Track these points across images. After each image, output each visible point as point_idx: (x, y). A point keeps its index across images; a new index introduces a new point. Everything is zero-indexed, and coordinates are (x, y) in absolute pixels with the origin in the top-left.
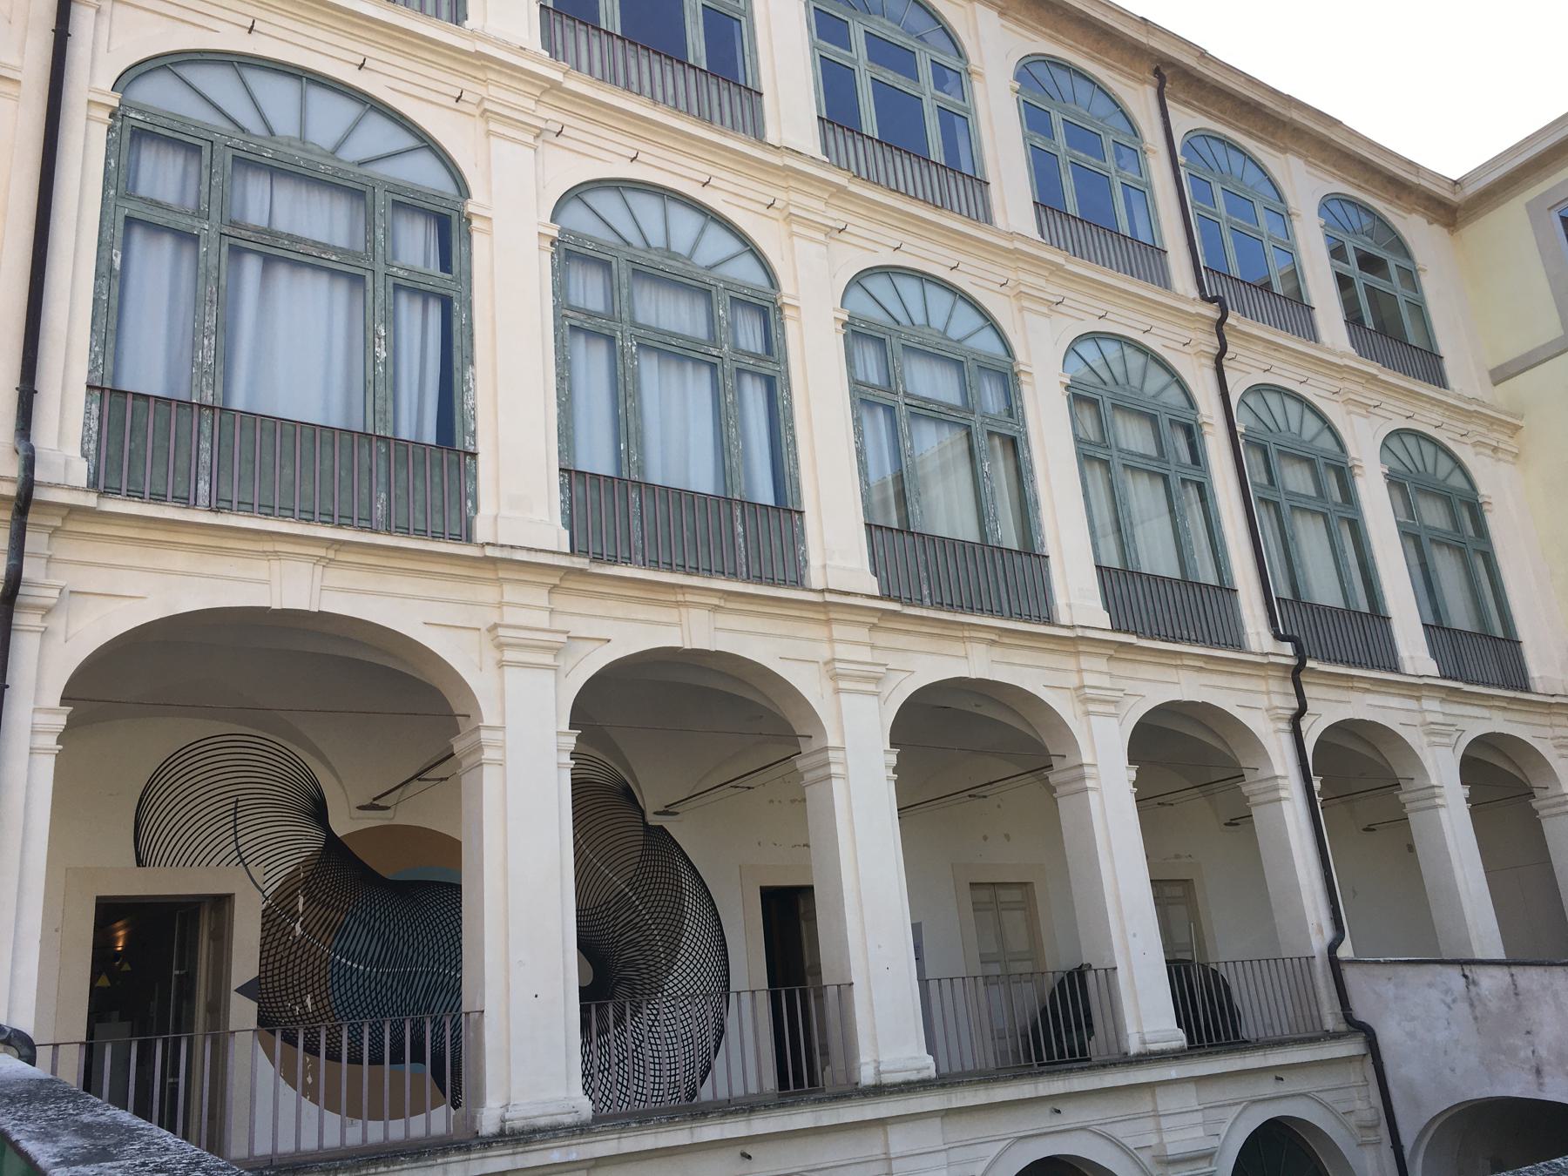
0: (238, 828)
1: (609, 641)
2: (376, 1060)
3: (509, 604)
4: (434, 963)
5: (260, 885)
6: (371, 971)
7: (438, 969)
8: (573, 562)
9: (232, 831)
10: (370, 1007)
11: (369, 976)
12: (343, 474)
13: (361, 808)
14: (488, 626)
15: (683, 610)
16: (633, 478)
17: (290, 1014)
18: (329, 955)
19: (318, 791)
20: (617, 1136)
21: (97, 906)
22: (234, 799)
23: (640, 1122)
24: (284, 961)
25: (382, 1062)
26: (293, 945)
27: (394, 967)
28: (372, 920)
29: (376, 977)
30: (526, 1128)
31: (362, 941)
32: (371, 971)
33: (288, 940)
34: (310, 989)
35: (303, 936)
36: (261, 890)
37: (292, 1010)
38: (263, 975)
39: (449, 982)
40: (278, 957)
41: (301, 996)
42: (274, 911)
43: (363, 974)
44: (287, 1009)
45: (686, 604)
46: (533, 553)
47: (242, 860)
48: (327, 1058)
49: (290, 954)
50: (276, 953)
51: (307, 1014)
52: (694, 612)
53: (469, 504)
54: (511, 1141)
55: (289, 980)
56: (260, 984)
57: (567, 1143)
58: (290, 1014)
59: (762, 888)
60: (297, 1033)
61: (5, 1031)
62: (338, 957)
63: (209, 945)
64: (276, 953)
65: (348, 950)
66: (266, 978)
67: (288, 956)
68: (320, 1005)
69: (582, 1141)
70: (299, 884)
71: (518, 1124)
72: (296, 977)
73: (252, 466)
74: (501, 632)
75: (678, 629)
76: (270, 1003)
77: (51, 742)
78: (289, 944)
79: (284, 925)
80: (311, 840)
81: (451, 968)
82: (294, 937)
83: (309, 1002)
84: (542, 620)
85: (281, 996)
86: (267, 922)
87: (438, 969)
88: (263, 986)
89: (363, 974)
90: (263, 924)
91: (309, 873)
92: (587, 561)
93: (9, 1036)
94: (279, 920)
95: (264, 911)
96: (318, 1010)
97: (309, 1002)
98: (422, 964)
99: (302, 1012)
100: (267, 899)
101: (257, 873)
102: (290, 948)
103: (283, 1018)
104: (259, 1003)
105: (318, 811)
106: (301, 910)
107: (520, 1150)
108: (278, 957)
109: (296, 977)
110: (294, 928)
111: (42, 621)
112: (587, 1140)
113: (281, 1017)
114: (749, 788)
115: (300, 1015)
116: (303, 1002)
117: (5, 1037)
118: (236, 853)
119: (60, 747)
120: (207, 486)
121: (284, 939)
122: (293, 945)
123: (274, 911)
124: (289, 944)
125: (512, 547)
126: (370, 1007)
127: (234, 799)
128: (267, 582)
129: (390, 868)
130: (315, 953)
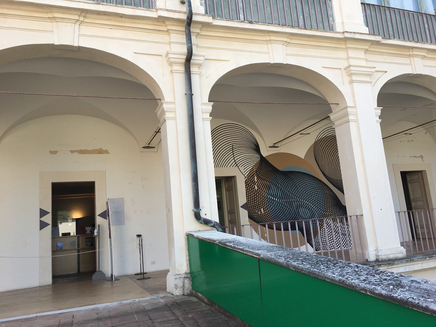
0: (234, 154)
1: (386, 72)
2: (286, 229)
3: (352, 58)
4: (298, 198)
5: (243, 173)
6: (279, 201)
7: (300, 200)
8: (376, 38)
9: (232, 156)
10: (281, 212)
11: (279, 202)
12: (287, 9)
13: (270, 147)
14: (344, 67)
15: (412, 59)
16: (386, 6)
17: (257, 214)
18: (266, 195)
19: (256, 142)
20: (422, 262)
21: (216, 180)
22: (232, 145)
23: (430, 257)
24: (253, 198)
25: (288, 230)
26: (255, 192)
27: (286, 199)
28: (278, 184)
29: (281, 203)
30: (387, 259)
31: (275, 191)
32: (279, 201)
33: (254, 191)
34: (262, 206)
35: (258, 190)
36: (243, 175)
37: (258, 213)
38: (248, 202)
39: (303, 204)
40: (251, 196)
41: (260, 209)
42: (248, 181)
43: (277, 201)
44: (256, 213)
45: (413, 56)
46: (362, 35)
47: (237, 165)
48: (276, 230)
49: (255, 195)
50: (251, 195)
51: (262, 214)
52: (416, 59)
53: (331, 19)
54: (387, 264)
55: (256, 203)
56: (247, 205)
57: (405, 265)
58: (257, 214)
59: (401, 172)
60: (288, 223)
61: (213, 222)
62: (269, 196)
63: (226, 193)
64: (251, 195)
65: (273, 195)
66: (249, 203)
67: (254, 196)
68: (266, 211)
69: (410, 264)
70: (254, 172)
71: (384, 257)
72: (258, 202)
73: (256, 7)
74: (352, 68)
75: (410, 66)
76: (251, 211)
77: (207, 116)
78: (254, 192)
79: (252, 186)
80: (256, 159)
81: (304, 200)
82: (255, 190)
83: (262, 210)
84: (363, 63)
85: (254, 209)
86: (247, 185)
87: (300, 200)
88: (248, 206)
89: (277, 201)
90: (246, 186)
91: (257, 169)
92: (381, 37)
93: (214, 224)
94: (250, 184)
95: (245, 181)
96: (265, 213)
97: (262, 210)
98: (294, 198)
99: (261, 214)
100: (246, 177)
101: (242, 169)
102: (255, 193)
103: (255, 216)
104: (248, 211)
105: (257, 149)
106: (256, 181)
107: (390, 267)
108: (251, 196)
109: (258, 202)
110: (255, 187)
111: (199, 70)
112: (412, 264)
113: (255, 215)
114: (410, 134)
115: (260, 215)
116: (261, 210)
117: (212, 224)
118: (234, 163)
119: (211, 118)
120: (243, 16)
121: (252, 190)
122: (255, 192)
123: (248, 181)
124: (254, 192)
125: (354, 33)
126: (281, 212)
127: (232, 145)
128: (268, 53)
129: (281, 168)
130: (262, 195)
